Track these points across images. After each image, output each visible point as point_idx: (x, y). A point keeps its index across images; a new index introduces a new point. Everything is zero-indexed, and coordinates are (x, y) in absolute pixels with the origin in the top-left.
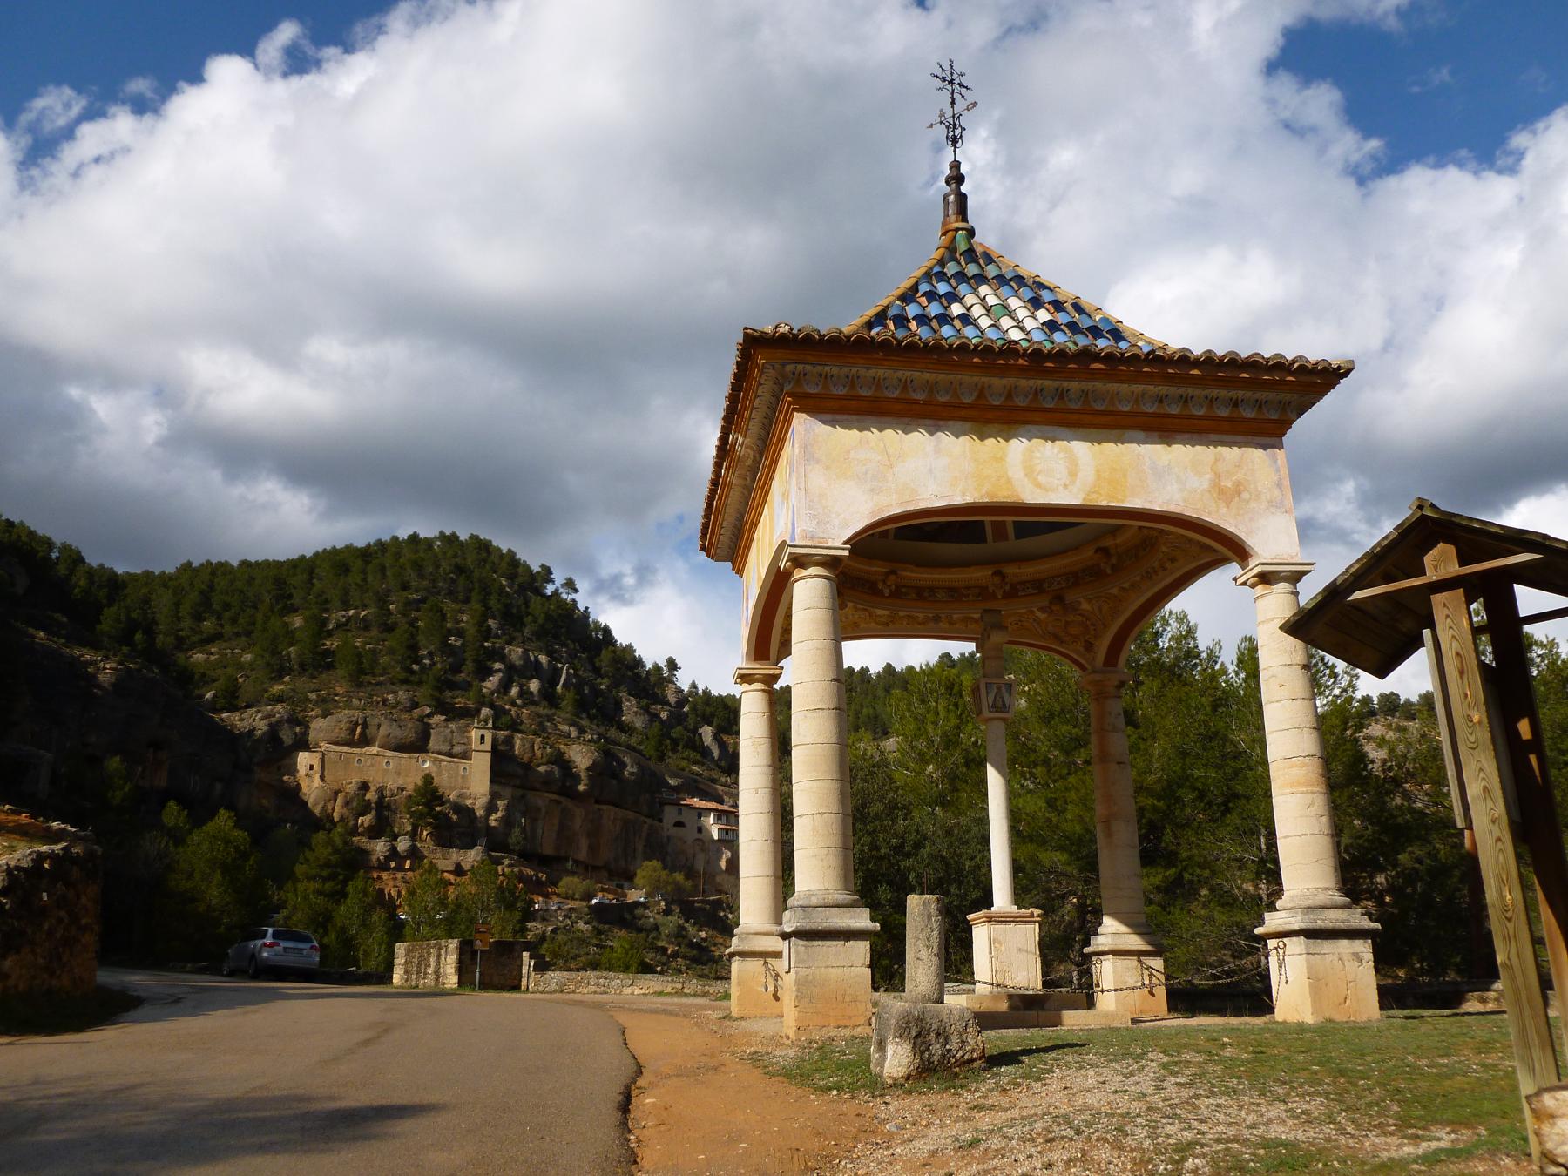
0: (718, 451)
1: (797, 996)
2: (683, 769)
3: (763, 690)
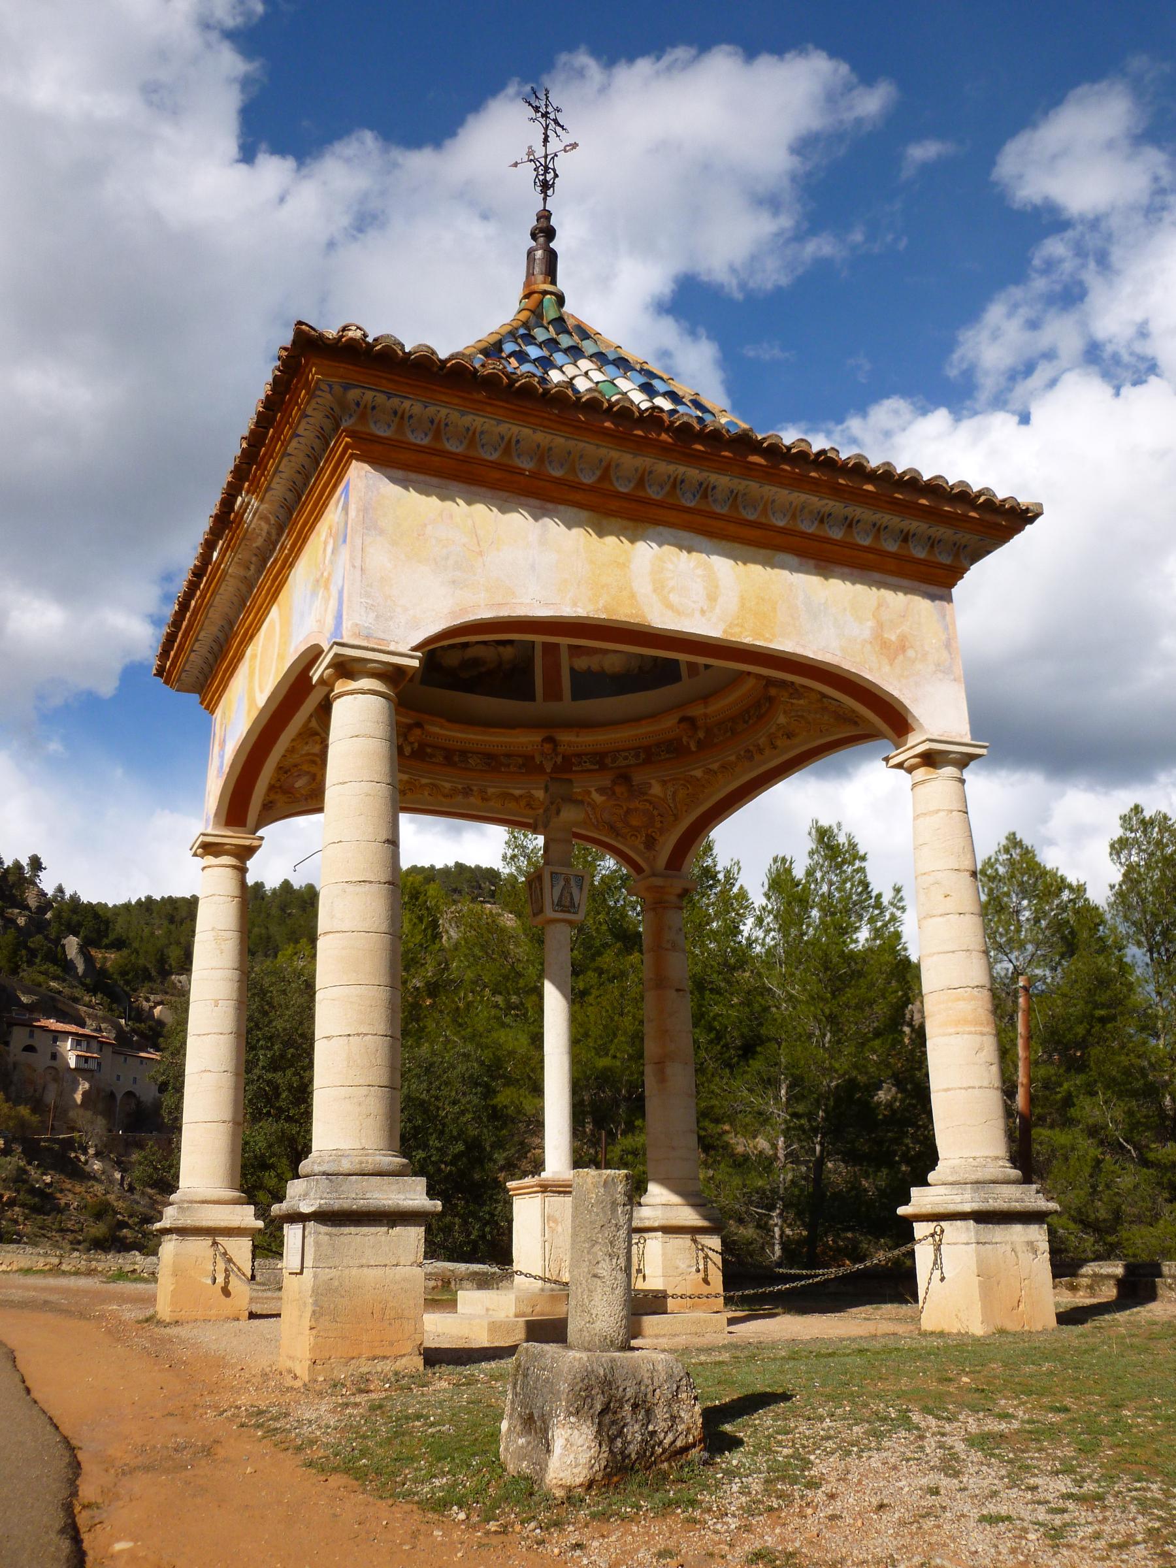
0: (215, 522)
1: (314, 1312)
2: (40, 985)
3: (234, 867)
